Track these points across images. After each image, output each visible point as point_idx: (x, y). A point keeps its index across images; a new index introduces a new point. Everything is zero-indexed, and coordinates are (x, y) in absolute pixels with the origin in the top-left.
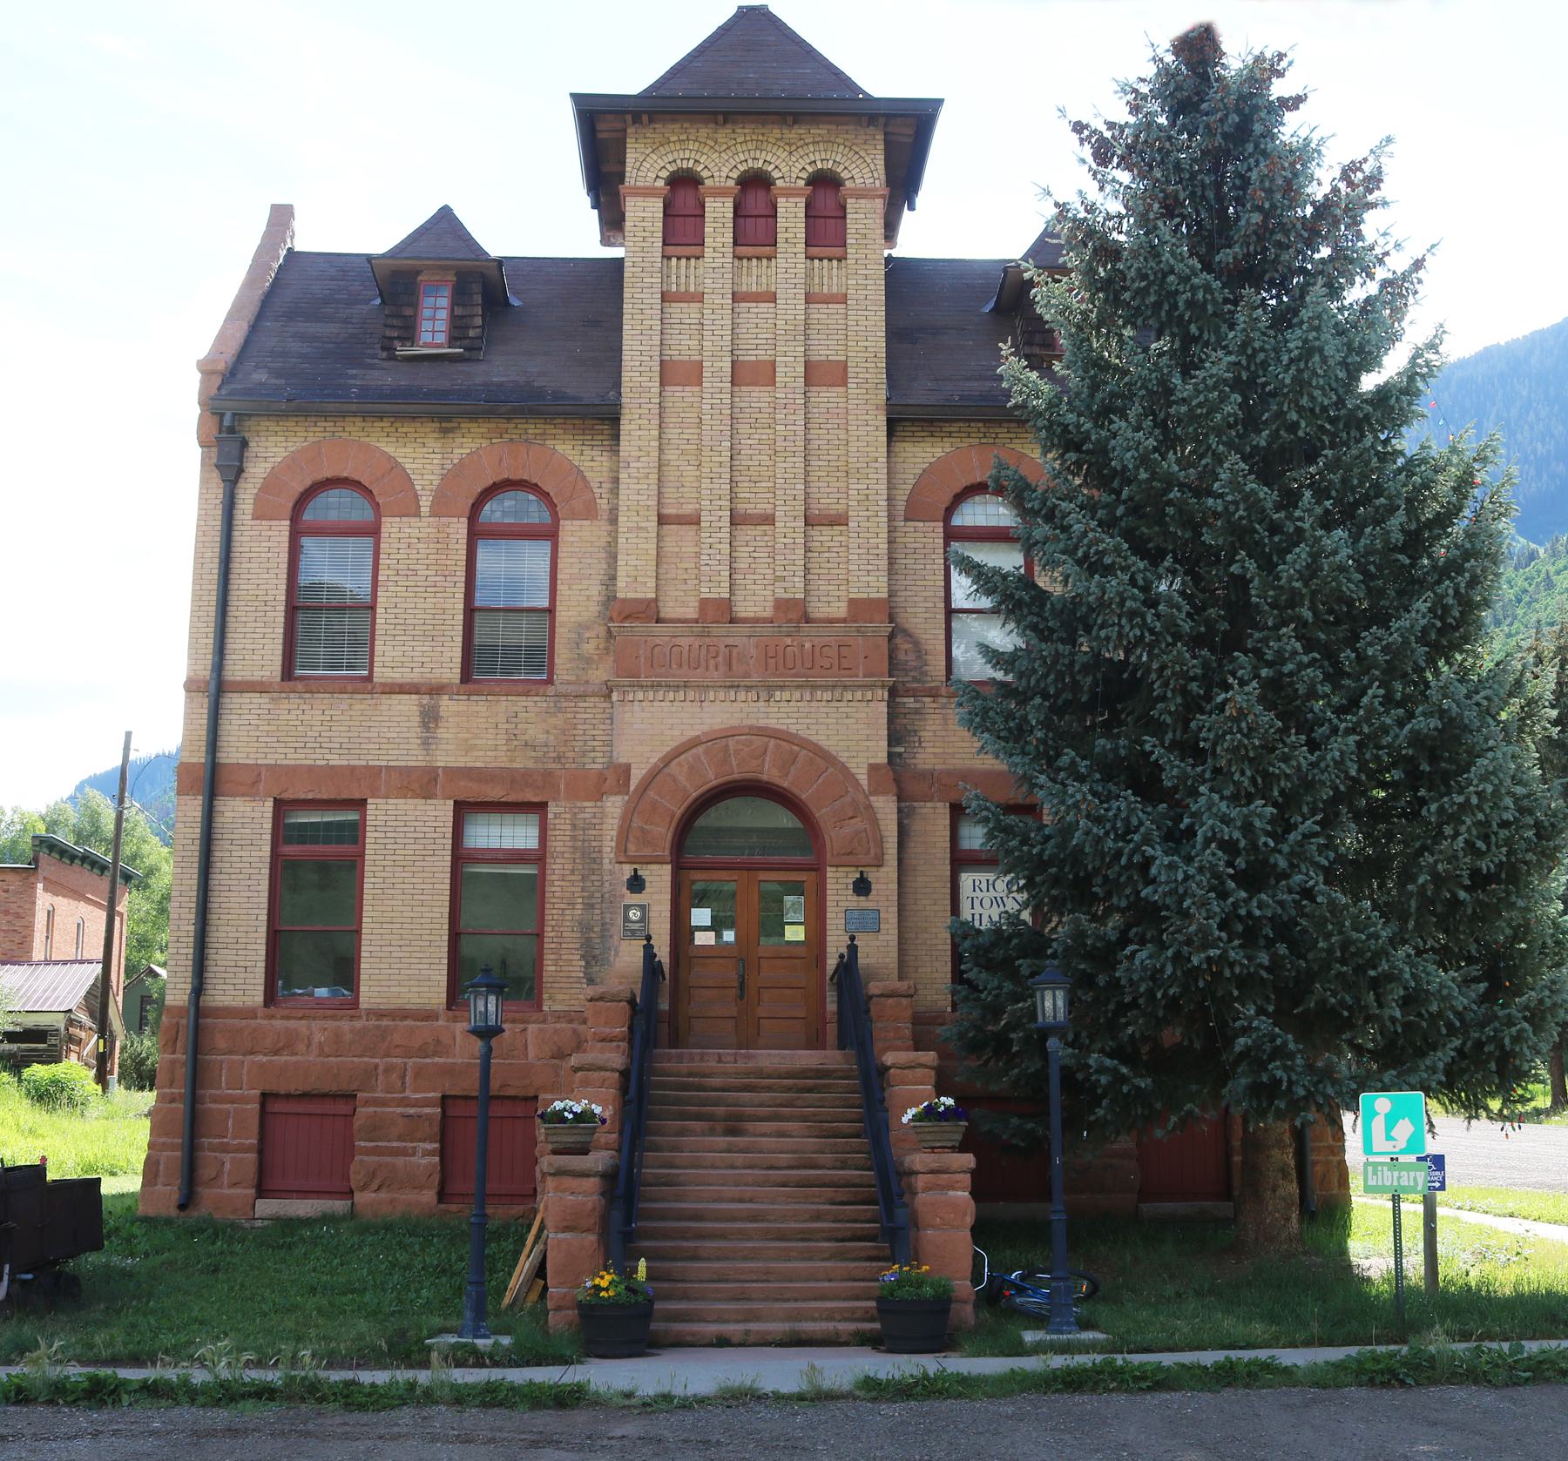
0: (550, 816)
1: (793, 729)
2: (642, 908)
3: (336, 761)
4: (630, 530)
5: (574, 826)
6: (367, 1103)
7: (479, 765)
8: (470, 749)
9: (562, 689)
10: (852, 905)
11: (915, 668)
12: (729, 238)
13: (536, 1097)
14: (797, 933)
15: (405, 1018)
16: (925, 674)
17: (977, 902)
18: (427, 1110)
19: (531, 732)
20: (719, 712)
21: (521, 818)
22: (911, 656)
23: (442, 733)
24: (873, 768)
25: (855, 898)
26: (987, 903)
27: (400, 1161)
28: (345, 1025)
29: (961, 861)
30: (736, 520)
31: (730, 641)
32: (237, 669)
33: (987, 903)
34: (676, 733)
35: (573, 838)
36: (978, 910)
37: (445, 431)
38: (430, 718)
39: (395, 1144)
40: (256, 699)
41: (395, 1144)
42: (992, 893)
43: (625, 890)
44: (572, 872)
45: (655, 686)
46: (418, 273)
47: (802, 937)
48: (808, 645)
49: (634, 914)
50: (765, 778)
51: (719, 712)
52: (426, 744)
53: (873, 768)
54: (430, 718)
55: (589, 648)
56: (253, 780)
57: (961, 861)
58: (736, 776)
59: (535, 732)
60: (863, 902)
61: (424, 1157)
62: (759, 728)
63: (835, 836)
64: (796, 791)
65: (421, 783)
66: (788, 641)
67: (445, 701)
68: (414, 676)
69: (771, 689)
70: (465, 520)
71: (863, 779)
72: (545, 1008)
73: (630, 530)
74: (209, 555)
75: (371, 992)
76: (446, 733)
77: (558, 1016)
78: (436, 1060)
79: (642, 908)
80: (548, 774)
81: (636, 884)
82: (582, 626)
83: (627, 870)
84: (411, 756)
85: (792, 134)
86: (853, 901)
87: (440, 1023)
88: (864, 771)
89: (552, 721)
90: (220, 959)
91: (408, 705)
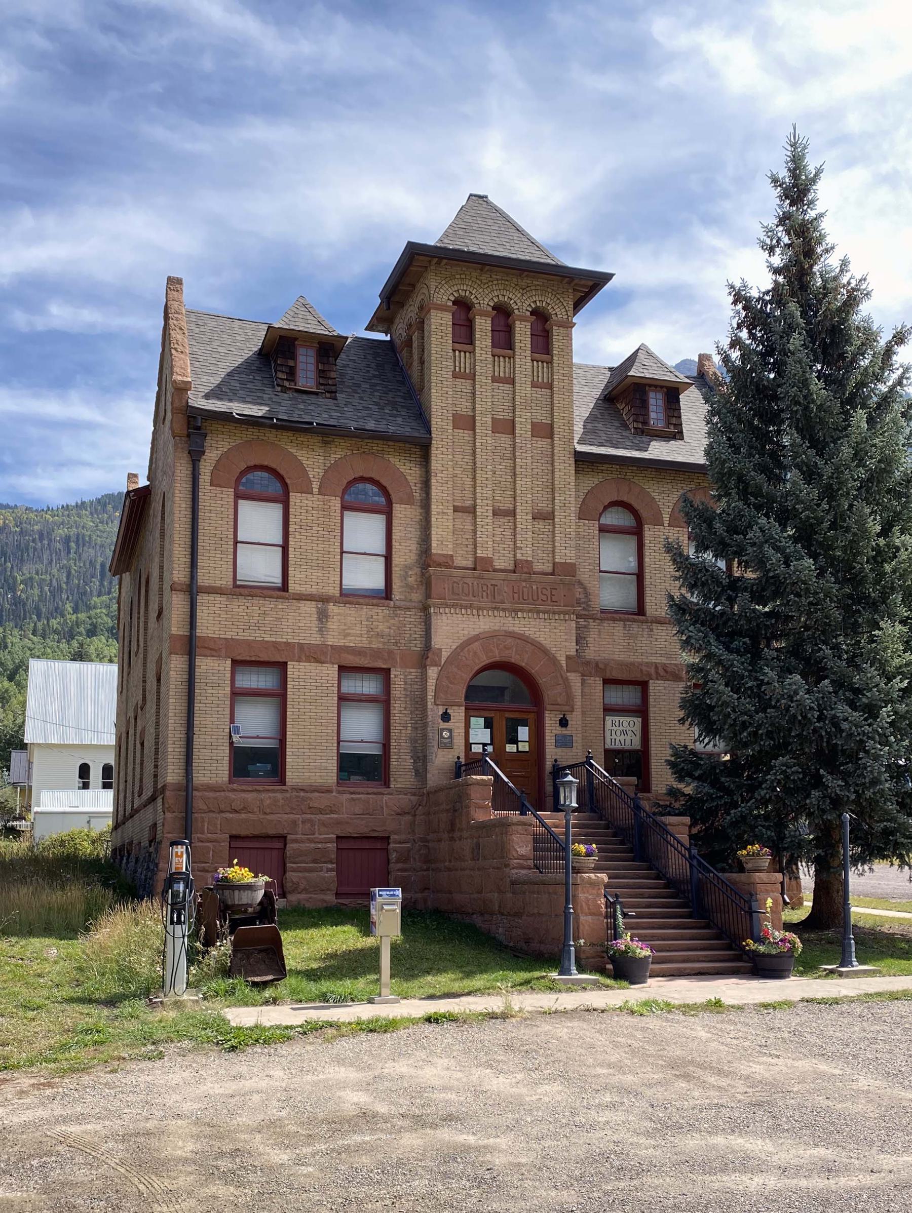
0: (392, 676)
1: (527, 633)
2: (450, 731)
3: (268, 638)
4: (438, 513)
5: (406, 684)
6: (296, 841)
7: (351, 645)
8: (346, 635)
9: (398, 603)
10: (559, 732)
11: (584, 603)
12: (489, 342)
13: (389, 838)
14: (524, 747)
15: (314, 791)
16: (589, 606)
17: (613, 732)
18: (329, 845)
19: (380, 627)
20: (485, 623)
21: (372, 676)
22: (582, 596)
23: (330, 625)
24: (568, 658)
25: (560, 728)
26: (618, 733)
27: (315, 874)
28: (279, 796)
29: (237, 694)
30: (513, 513)
31: (493, 582)
32: (203, 579)
33: (618, 733)
34: (466, 632)
35: (405, 689)
36: (614, 736)
37: (326, 443)
38: (323, 616)
39: (311, 865)
40: (218, 598)
41: (311, 865)
42: (621, 728)
43: (440, 720)
44: (405, 708)
45: (454, 606)
46: (296, 339)
47: (527, 749)
48: (534, 587)
49: (445, 734)
50: (513, 661)
51: (485, 623)
52: (321, 631)
53: (568, 658)
54: (323, 616)
55: (411, 580)
56: (215, 648)
57: (237, 694)
58: (497, 659)
59: (382, 627)
60: (564, 731)
61: (328, 873)
62: (510, 632)
63: (551, 693)
64: (528, 668)
65: (314, 654)
66: (524, 584)
67: (331, 606)
68: (314, 590)
69: (516, 611)
70: (338, 499)
71: (564, 663)
72: (392, 786)
73: (438, 513)
74: (184, 506)
75: (292, 775)
76: (333, 625)
77: (400, 792)
78: (332, 816)
79: (450, 731)
80: (390, 652)
81: (446, 717)
82: (407, 568)
83: (441, 710)
84: (314, 639)
85: (524, 282)
86: (559, 730)
87: (334, 794)
88: (564, 659)
89: (392, 621)
90: (200, 755)
91: (309, 608)
